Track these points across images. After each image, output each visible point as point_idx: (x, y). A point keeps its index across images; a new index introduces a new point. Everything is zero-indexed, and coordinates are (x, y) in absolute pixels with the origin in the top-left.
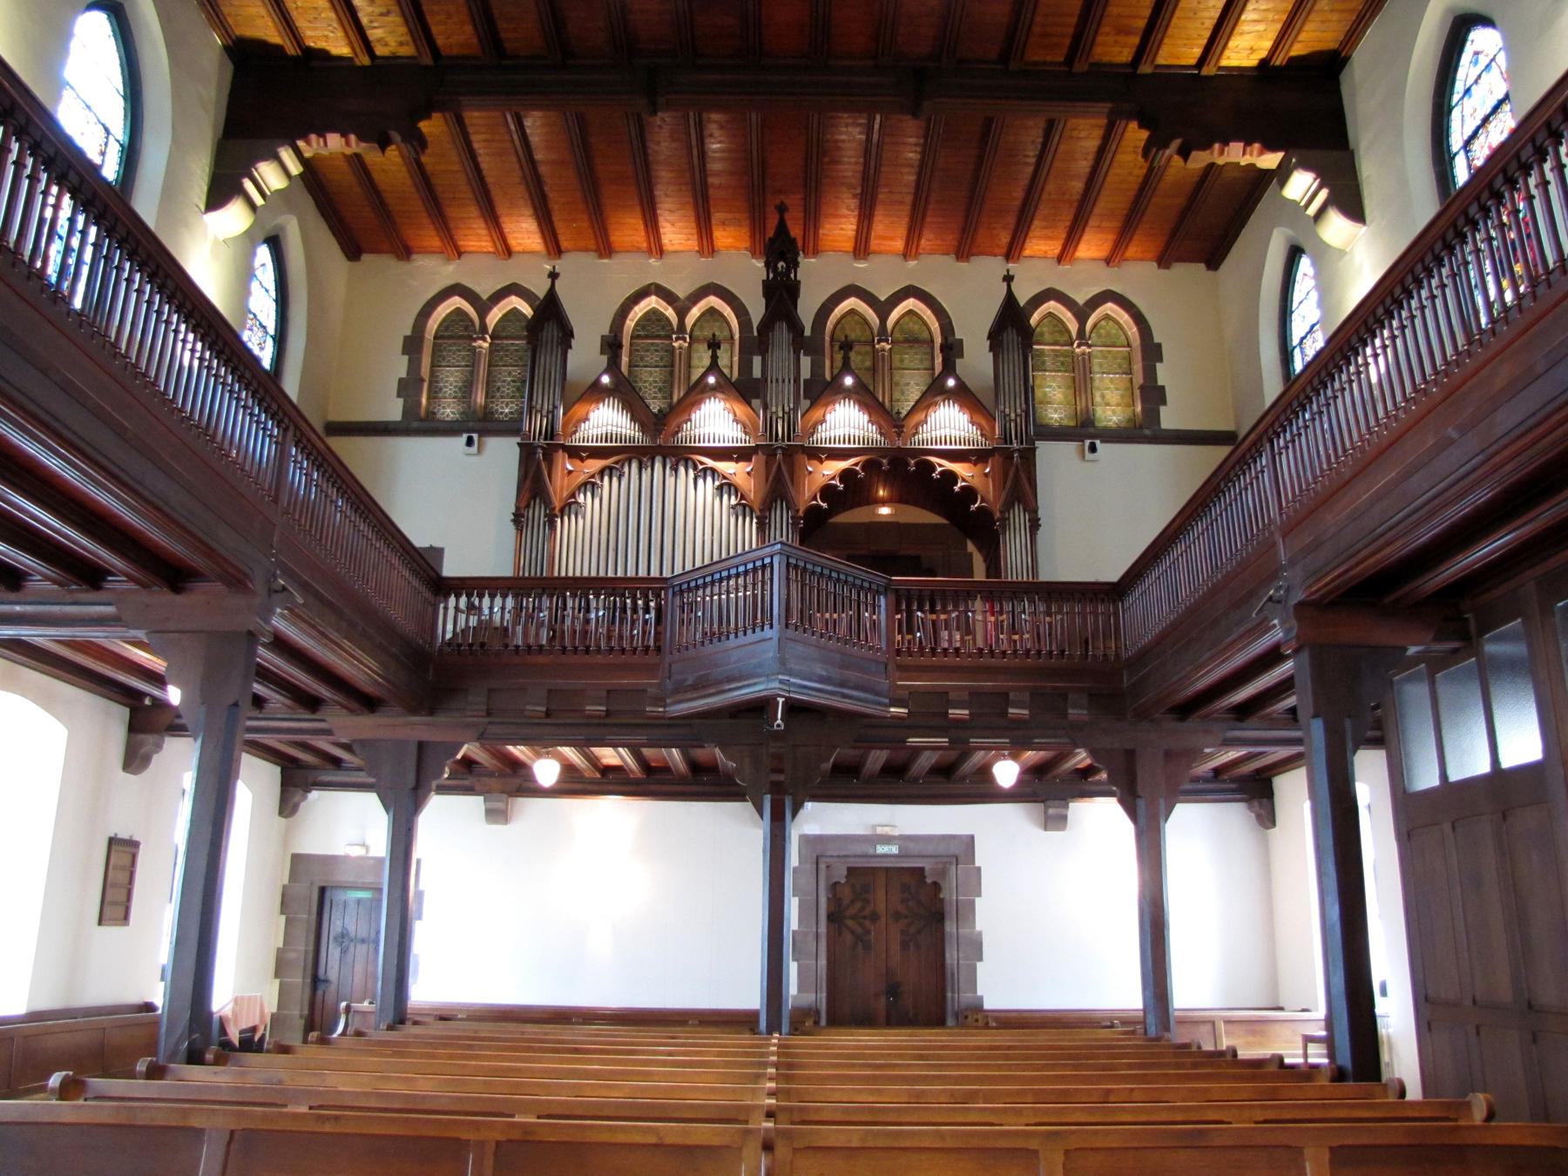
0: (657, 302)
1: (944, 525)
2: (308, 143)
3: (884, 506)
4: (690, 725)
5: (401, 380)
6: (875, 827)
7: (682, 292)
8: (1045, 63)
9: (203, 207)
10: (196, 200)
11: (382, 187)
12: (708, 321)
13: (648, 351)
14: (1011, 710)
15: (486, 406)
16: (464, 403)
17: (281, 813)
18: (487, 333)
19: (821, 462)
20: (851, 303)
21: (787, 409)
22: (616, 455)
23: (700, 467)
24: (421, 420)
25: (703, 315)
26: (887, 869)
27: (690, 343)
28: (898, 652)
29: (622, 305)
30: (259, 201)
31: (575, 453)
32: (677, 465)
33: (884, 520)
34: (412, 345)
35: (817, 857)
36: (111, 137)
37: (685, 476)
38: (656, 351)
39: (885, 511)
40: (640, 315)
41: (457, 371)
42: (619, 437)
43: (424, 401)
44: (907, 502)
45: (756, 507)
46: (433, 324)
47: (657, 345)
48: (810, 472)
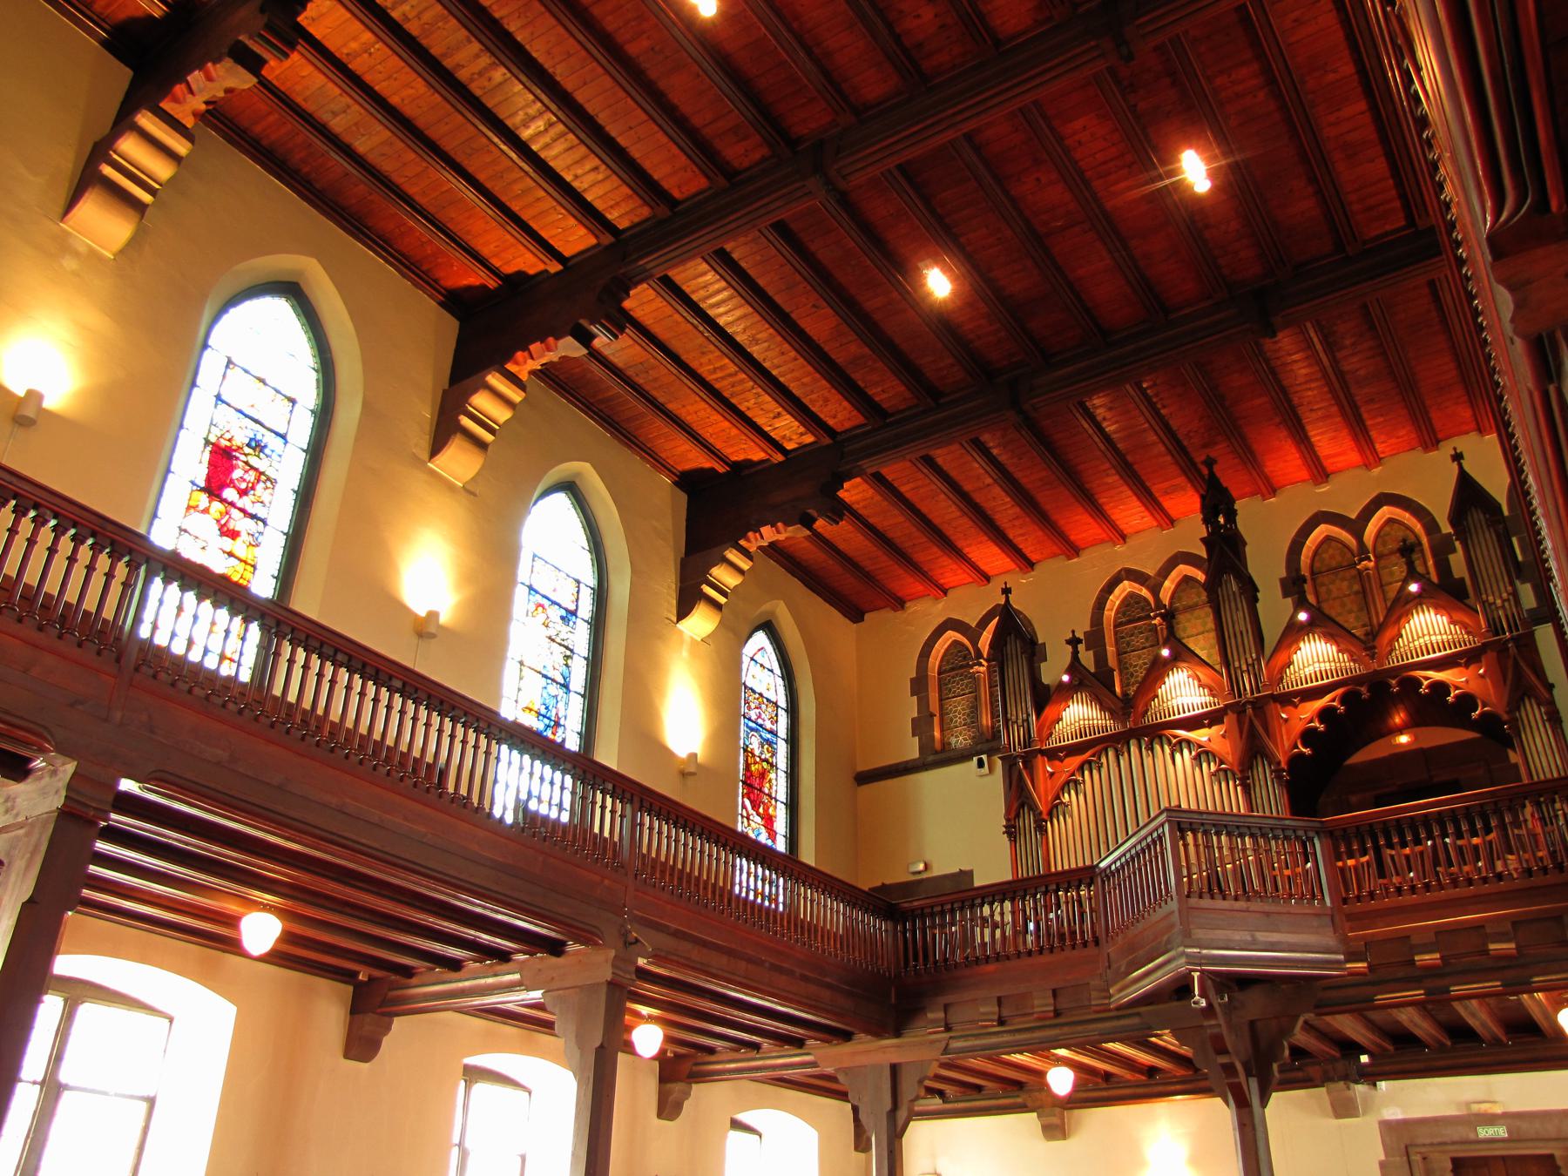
0: (1130, 586)
1: (1478, 738)
2: (748, 540)
3: (1402, 734)
4: (1138, 1014)
5: (913, 720)
6: (1468, 1104)
7: (1151, 571)
8: (1386, 234)
9: (675, 619)
10: (666, 614)
11: (851, 553)
12: (1184, 591)
13: (1132, 635)
14: (1492, 946)
15: (993, 727)
16: (973, 727)
17: (857, 1148)
18: (982, 657)
19: (1296, 706)
20: (1322, 530)
21: (1250, 661)
22: (1090, 748)
23: (1174, 741)
24: (937, 753)
25: (1178, 585)
26: (1503, 1158)
27: (1376, 562)
28: (1345, 901)
29: (1098, 598)
30: (722, 600)
31: (1052, 755)
32: (1152, 744)
33: (1407, 749)
34: (919, 685)
35: (1406, 1147)
36: (582, 586)
37: (1162, 752)
38: (1142, 633)
39: (1404, 739)
40: (1117, 603)
41: (963, 700)
42: (1093, 729)
43: (937, 734)
44: (1426, 724)
45: (1236, 769)
46: (1110, 613)
47: (1140, 627)
48: (1286, 720)
